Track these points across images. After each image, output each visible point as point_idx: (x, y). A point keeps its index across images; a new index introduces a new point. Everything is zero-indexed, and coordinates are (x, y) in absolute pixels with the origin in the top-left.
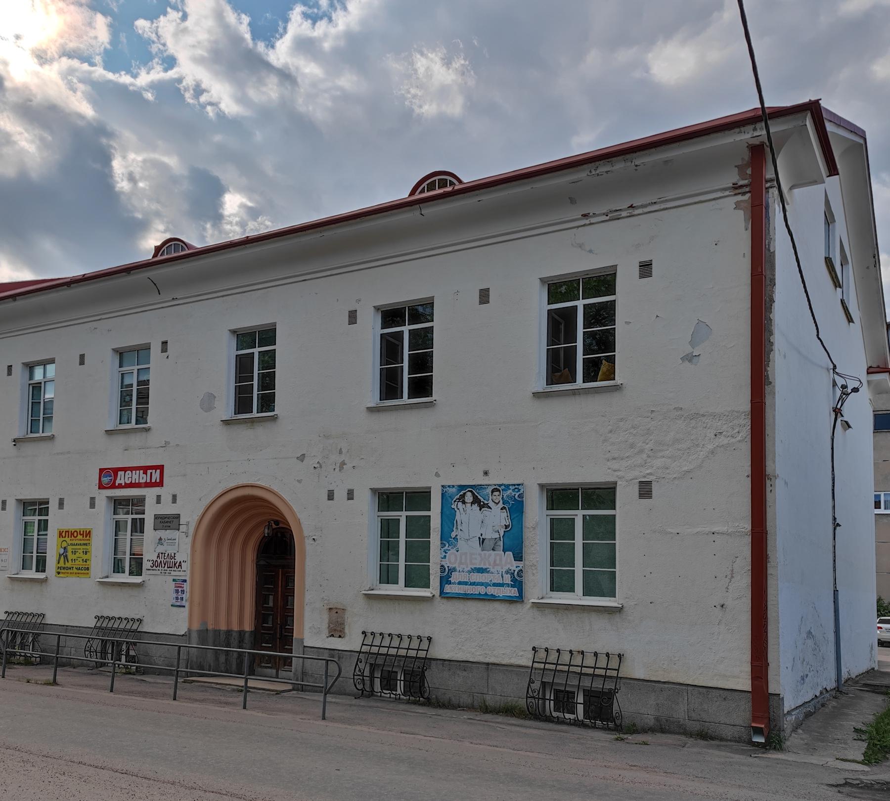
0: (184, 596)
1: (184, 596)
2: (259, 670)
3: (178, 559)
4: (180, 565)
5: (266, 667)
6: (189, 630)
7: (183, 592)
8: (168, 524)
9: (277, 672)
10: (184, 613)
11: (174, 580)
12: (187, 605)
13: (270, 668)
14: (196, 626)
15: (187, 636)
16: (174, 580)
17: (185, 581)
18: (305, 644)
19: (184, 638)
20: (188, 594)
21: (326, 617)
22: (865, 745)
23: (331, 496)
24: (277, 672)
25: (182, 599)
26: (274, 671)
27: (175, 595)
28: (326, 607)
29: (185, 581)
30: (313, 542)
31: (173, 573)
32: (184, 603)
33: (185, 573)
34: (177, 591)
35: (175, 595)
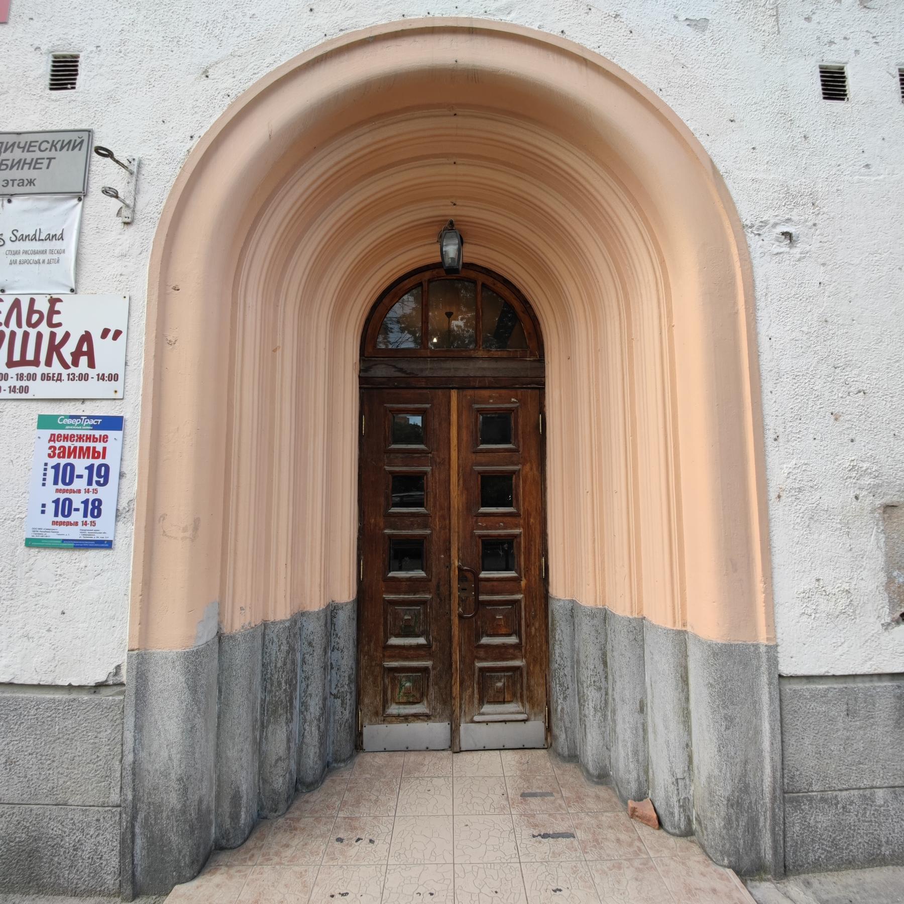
0: (106, 494)
1: (106, 494)
2: (374, 732)
3: (74, 321)
4: (86, 348)
5: (406, 718)
6: (141, 661)
7: (101, 475)
8: (26, 173)
9: (454, 732)
10: (109, 579)
11: (45, 422)
12: (127, 537)
13: (427, 717)
14: (177, 633)
15: (127, 690)
16: (45, 422)
17: (115, 423)
18: (786, 669)
19: (107, 697)
20: (132, 487)
21: (871, 542)
22: (669, 626)
23: (834, 84)
24: (454, 732)
25: (94, 509)
26: (438, 730)
27: (50, 493)
28: (868, 501)
29: (115, 423)
30: (784, 247)
31: (38, 389)
32: (104, 527)
33: (121, 382)
34: (65, 475)
35: (50, 493)
